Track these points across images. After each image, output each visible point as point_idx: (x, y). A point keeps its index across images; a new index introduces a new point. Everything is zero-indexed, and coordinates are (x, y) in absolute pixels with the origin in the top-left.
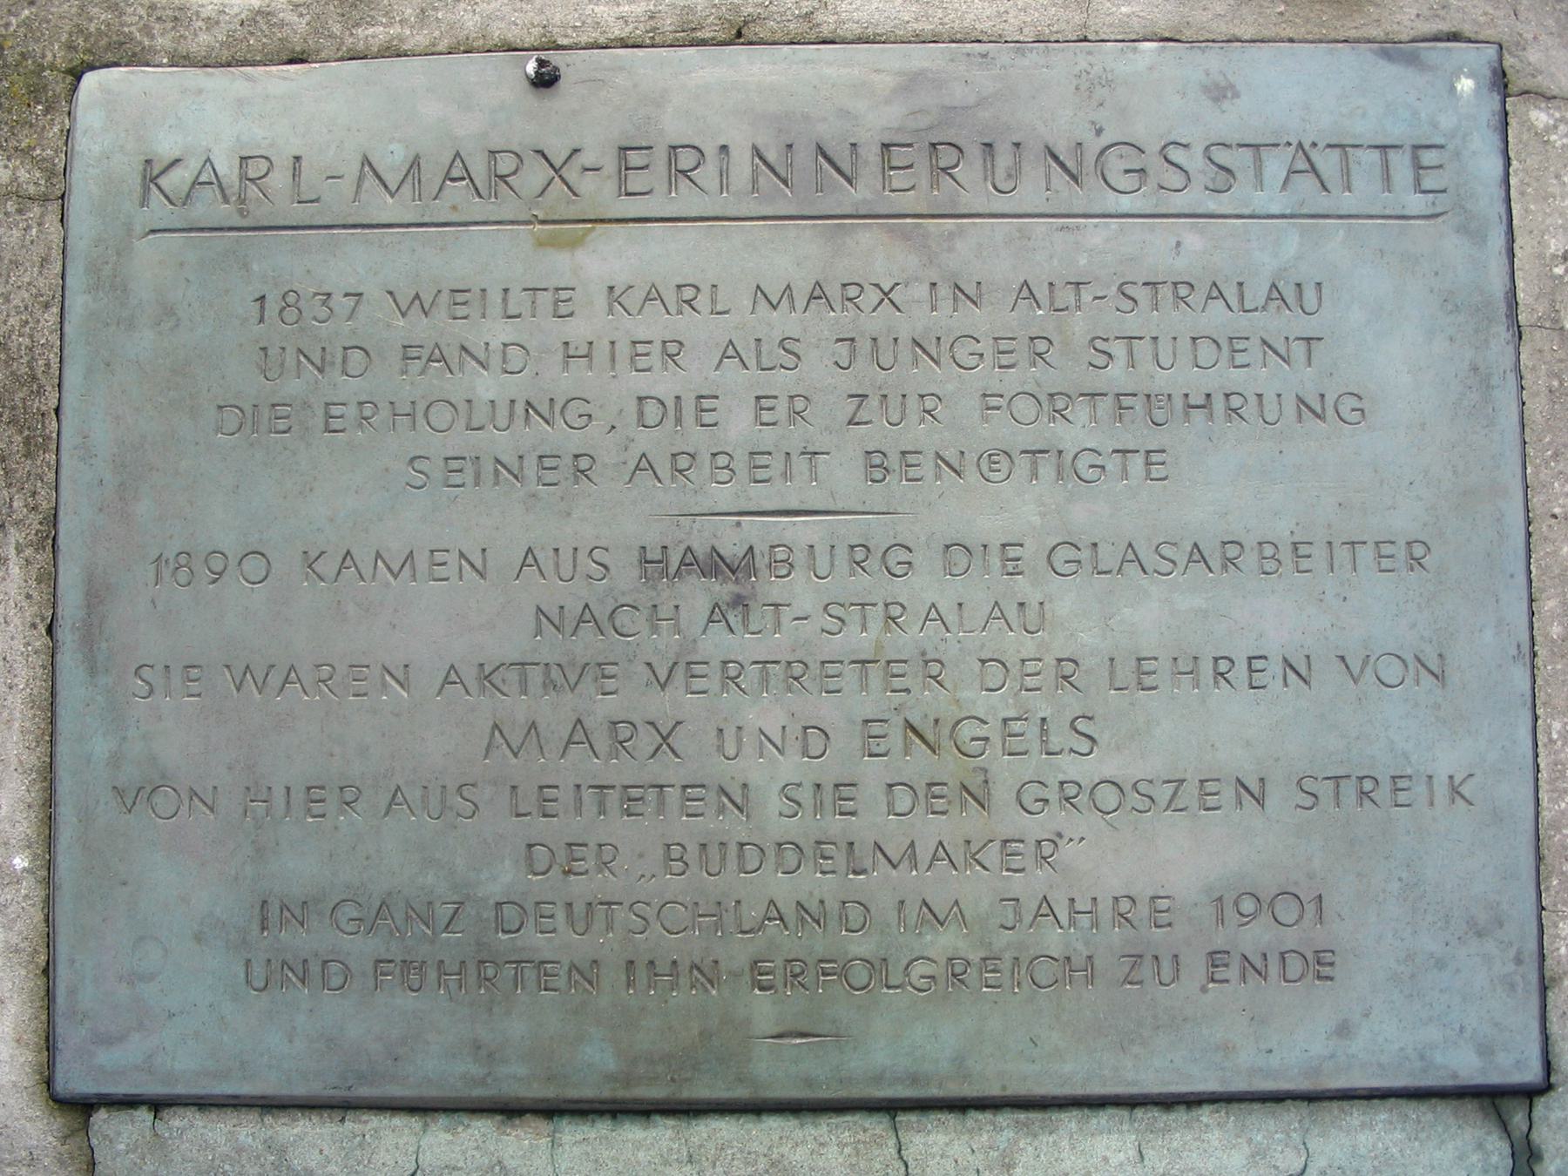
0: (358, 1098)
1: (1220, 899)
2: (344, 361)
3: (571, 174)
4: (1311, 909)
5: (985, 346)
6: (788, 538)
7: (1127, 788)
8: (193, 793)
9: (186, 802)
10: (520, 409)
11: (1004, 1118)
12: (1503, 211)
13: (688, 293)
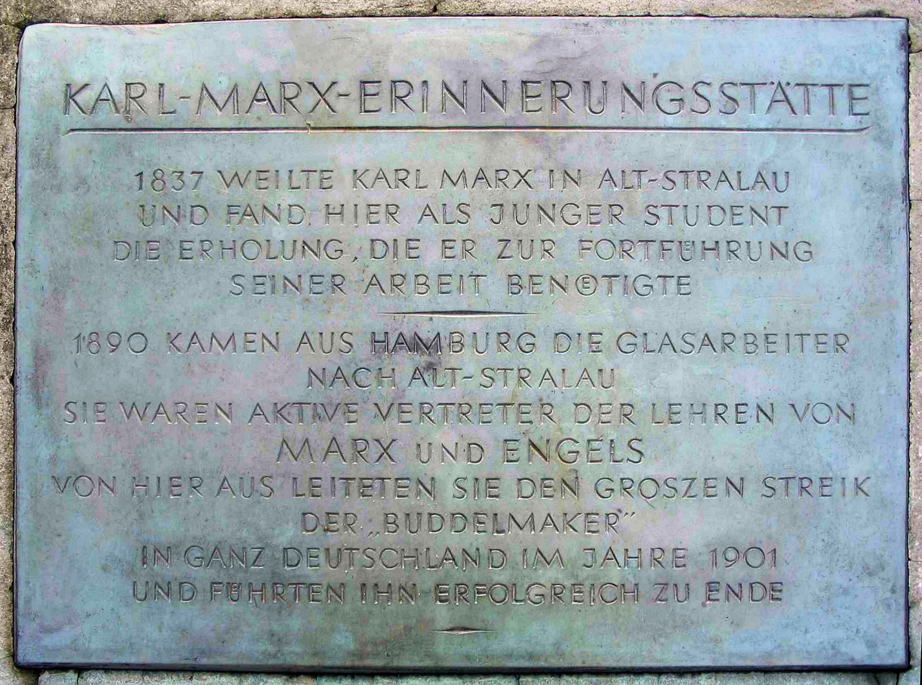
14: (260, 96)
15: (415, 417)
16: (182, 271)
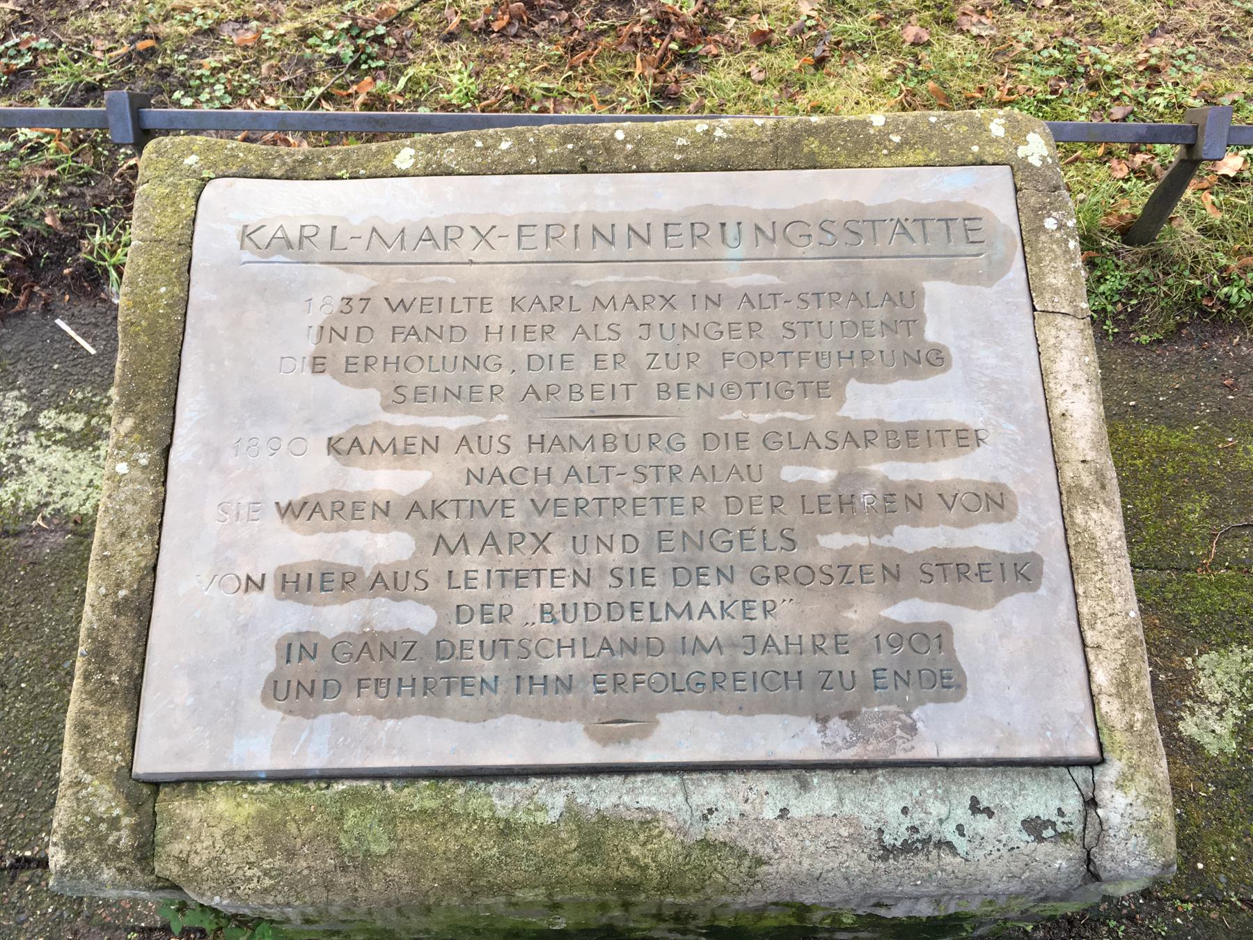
5: (724, 327)
6: (614, 431)
13: (556, 300)
14: (606, 646)
15: (476, 690)
16: (714, 651)
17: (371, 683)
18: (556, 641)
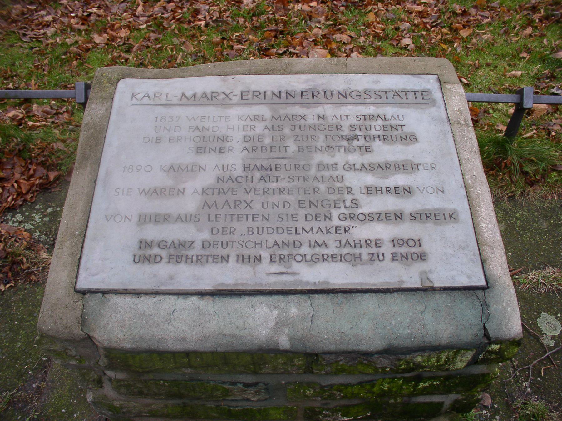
0: (160, 290)
1: (393, 241)
2: (175, 129)
3: (230, 96)
4: (417, 243)
7: (367, 216)
8: (126, 217)
9: (124, 218)
10: (216, 138)
11: (340, 295)
12: (443, 102)
17: (175, 257)
18: (254, 242)
